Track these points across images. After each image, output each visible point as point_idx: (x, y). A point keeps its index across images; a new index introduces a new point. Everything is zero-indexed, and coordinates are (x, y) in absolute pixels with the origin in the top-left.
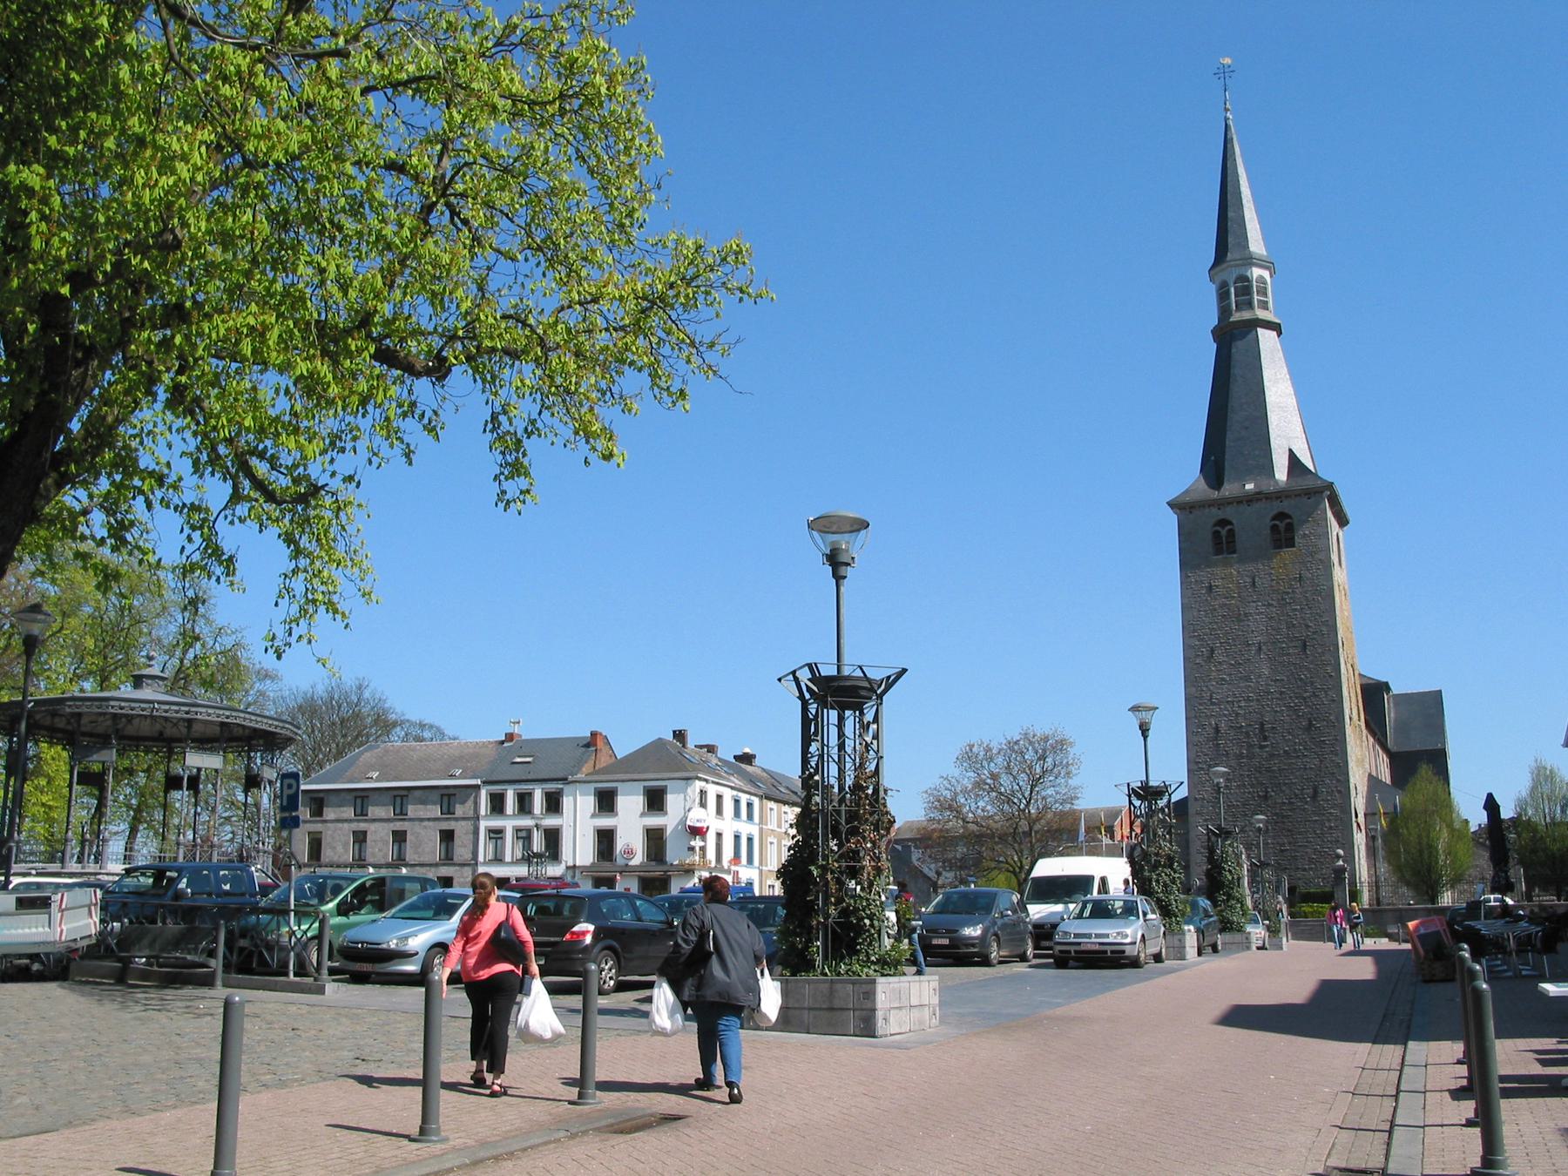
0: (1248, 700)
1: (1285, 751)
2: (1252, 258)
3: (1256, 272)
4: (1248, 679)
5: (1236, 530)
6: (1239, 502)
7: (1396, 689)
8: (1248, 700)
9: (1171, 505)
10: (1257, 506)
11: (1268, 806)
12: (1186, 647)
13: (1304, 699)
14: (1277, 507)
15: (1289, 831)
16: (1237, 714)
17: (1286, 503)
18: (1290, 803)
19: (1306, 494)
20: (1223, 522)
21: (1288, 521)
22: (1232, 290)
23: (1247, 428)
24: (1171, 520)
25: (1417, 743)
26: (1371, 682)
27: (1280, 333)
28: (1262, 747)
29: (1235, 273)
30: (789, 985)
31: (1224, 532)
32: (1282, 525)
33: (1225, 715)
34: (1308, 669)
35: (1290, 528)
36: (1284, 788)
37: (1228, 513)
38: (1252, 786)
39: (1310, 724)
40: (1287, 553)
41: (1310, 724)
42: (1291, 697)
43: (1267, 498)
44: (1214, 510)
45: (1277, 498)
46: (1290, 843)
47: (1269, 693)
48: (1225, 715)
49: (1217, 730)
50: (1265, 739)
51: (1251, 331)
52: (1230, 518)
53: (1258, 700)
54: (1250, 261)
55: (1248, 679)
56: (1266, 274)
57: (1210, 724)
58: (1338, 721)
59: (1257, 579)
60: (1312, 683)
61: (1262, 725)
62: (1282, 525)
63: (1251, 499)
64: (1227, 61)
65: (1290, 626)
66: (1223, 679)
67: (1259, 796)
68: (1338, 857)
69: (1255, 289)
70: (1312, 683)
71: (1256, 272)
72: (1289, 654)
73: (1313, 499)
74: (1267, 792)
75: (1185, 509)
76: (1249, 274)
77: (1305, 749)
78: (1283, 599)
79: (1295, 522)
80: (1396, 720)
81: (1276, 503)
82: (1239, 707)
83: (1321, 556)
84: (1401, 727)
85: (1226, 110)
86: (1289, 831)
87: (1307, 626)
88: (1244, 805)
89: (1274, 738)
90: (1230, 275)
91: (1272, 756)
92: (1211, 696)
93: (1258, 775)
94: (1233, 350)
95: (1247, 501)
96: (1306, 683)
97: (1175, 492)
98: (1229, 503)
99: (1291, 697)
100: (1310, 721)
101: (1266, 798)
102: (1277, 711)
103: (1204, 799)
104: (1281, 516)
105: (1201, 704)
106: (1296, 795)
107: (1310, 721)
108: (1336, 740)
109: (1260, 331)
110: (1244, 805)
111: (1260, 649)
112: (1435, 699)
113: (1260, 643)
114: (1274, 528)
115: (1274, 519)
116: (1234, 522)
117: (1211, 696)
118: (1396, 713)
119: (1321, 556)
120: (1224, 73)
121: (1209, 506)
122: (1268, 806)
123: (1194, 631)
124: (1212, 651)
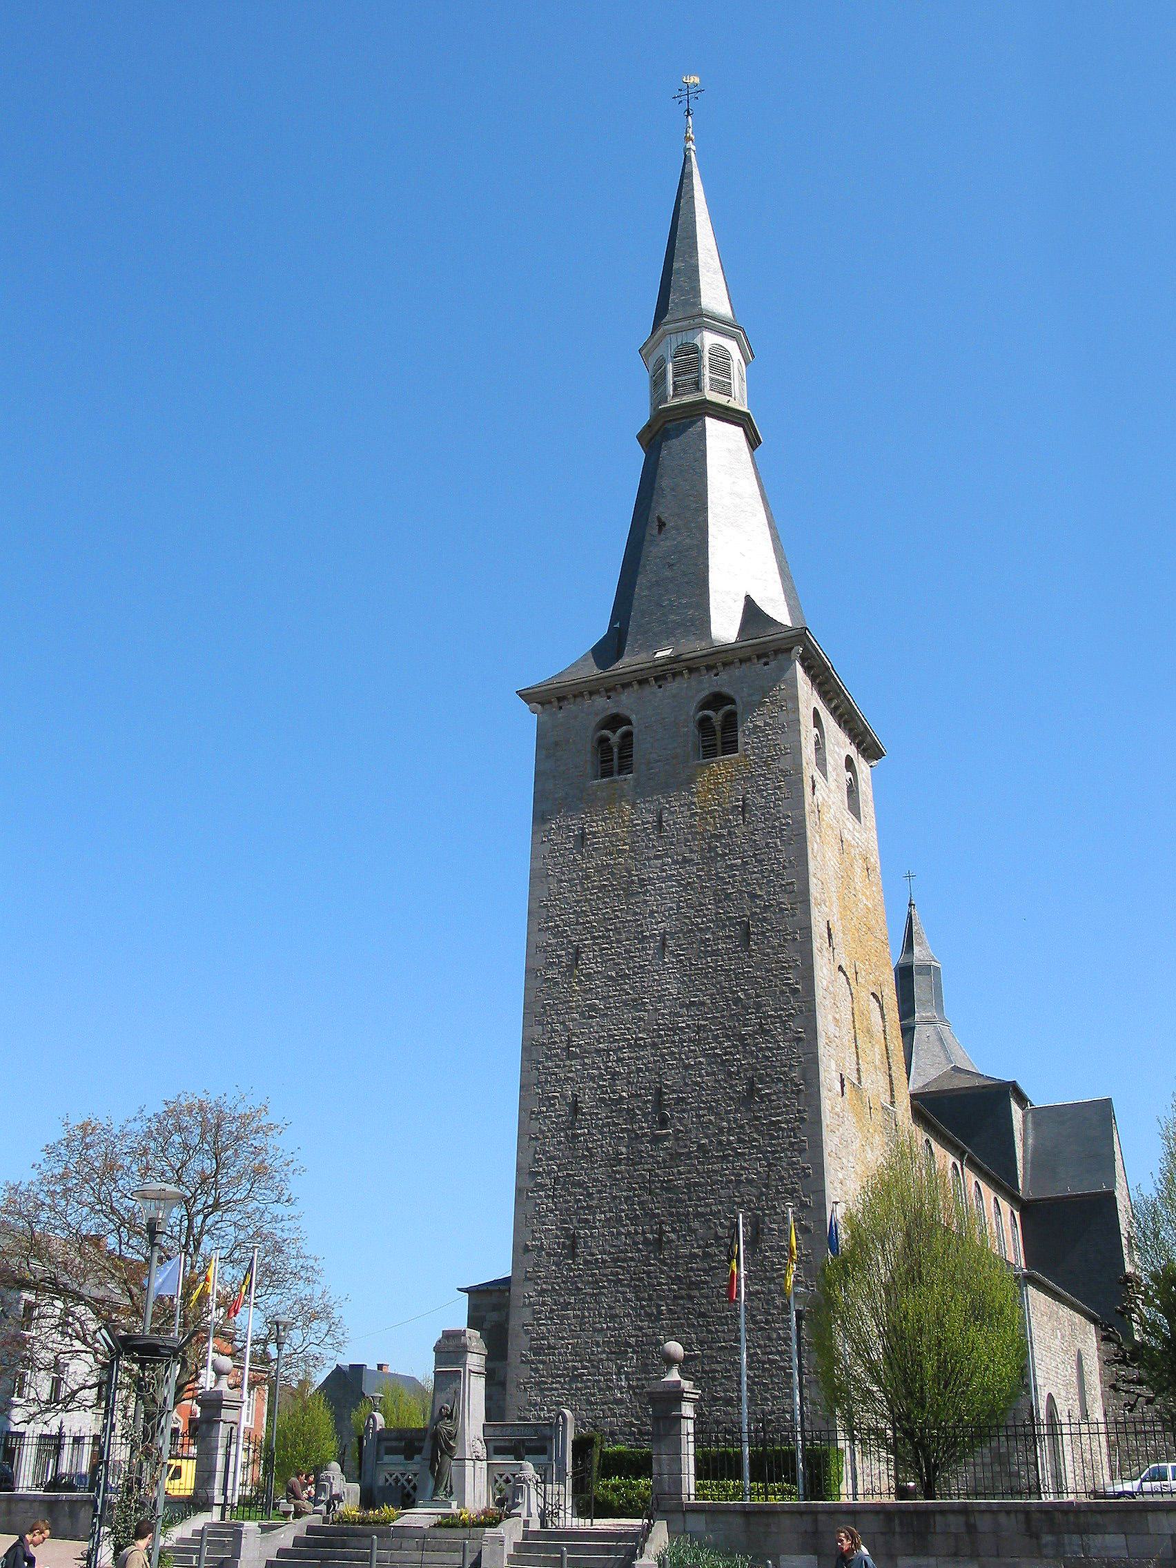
0: (636, 1046)
1: (700, 1146)
2: (701, 315)
3: (709, 340)
4: (637, 1004)
5: (635, 731)
6: (642, 682)
7: (1039, 1099)
8: (636, 1046)
9: (527, 696)
10: (673, 686)
11: (663, 1262)
12: (534, 949)
13: (742, 1038)
14: (709, 684)
15: (703, 1315)
16: (615, 1075)
17: (724, 676)
18: (706, 1255)
21: (729, 707)
22: (670, 367)
23: (671, 566)
24: (527, 721)
25: (1069, 1186)
26: (977, 1082)
27: (753, 441)
28: (656, 1140)
29: (675, 341)
30: (682, 1528)
31: (615, 738)
32: (717, 717)
33: (592, 1078)
34: (753, 981)
35: (731, 722)
36: (695, 1224)
37: (625, 703)
38: (634, 1219)
39: (752, 1090)
40: (722, 765)
41: (752, 1090)
42: (716, 1038)
43: (691, 670)
44: (600, 701)
45: (709, 668)
46: (701, 1343)
47: (675, 1029)
48: (592, 1078)
49: (575, 1108)
50: (664, 1122)
51: (692, 423)
52: (626, 712)
53: (654, 1045)
54: (700, 319)
55: (637, 1004)
56: (731, 346)
57: (564, 1097)
58: (806, 1083)
59: (665, 815)
60: (758, 1006)
61: (659, 1093)
62: (717, 717)
63: (662, 674)
64: (695, 79)
65: (722, 898)
66: (593, 1007)
67: (646, 1242)
68: (670, 1360)
69: (706, 362)
70: (758, 1006)
71: (709, 340)
72: (715, 953)
73: (773, 664)
74: (662, 1233)
76: (697, 341)
77: (740, 1141)
78: (712, 849)
79: (740, 709)
80: (1036, 1149)
82: (619, 1060)
83: (785, 763)
84: (1041, 1161)
85: (688, 139)
86: (703, 1315)
87: (753, 896)
88: (615, 1260)
89: (680, 1120)
90: (669, 347)
91: (675, 1156)
92: (570, 1041)
93: (646, 1197)
94: (664, 453)
95: (657, 679)
96: (746, 1008)
97: (541, 673)
98: (625, 686)
99: (716, 1038)
100: (751, 1083)
101: (659, 1244)
102: (687, 1067)
103: (541, 1248)
104: (717, 700)
105: (548, 1058)
106: (718, 1238)
107: (751, 1083)
108: (802, 1120)
109: (710, 423)
110: (615, 1260)
111: (664, 945)
112: (1101, 1113)
113: (663, 936)
114: (704, 724)
115: (706, 705)
116: (633, 717)
117: (570, 1041)
118: (1036, 1138)
119: (785, 763)
120: (688, 93)
121: (591, 693)
122: (663, 1262)
123: (550, 918)
124: (578, 953)
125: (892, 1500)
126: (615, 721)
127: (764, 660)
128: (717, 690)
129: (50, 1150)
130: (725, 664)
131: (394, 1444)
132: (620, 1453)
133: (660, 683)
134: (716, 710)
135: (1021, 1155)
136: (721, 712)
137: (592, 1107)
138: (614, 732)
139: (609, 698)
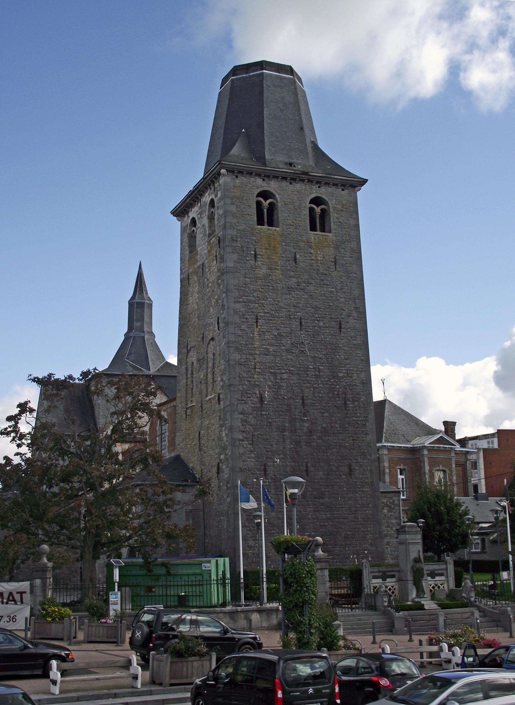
6: (284, 178)
10: (298, 186)
17: (323, 189)
19: (342, 185)
20: (265, 195)
43: (309, 181)
49: (261, 399)
73: (346, 191)
75: (233, 172)
81: (315, 187)
115: (312, 201)
125: (281, 648)
126: (317, 201)
127: (343, 188)
128: (320, 195)
129: (95, 369)
130: (326, 184)
131: (377, 574)
132: (173, 615)
133: (292, 181)
134: (266, 200)
135: (480, 460)
136: (320, 208)
137: (269, 401)
138: (266, 200)
139: (291, 184)
